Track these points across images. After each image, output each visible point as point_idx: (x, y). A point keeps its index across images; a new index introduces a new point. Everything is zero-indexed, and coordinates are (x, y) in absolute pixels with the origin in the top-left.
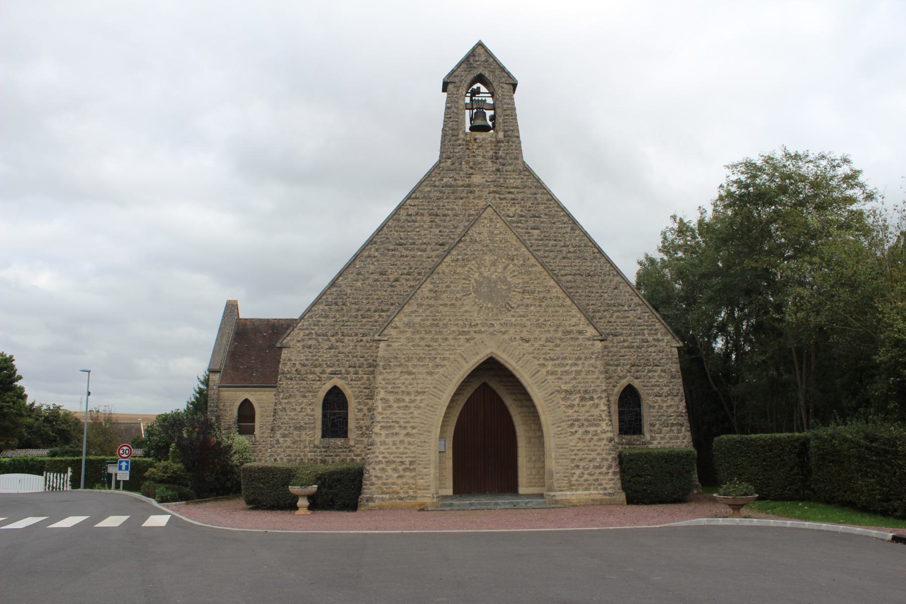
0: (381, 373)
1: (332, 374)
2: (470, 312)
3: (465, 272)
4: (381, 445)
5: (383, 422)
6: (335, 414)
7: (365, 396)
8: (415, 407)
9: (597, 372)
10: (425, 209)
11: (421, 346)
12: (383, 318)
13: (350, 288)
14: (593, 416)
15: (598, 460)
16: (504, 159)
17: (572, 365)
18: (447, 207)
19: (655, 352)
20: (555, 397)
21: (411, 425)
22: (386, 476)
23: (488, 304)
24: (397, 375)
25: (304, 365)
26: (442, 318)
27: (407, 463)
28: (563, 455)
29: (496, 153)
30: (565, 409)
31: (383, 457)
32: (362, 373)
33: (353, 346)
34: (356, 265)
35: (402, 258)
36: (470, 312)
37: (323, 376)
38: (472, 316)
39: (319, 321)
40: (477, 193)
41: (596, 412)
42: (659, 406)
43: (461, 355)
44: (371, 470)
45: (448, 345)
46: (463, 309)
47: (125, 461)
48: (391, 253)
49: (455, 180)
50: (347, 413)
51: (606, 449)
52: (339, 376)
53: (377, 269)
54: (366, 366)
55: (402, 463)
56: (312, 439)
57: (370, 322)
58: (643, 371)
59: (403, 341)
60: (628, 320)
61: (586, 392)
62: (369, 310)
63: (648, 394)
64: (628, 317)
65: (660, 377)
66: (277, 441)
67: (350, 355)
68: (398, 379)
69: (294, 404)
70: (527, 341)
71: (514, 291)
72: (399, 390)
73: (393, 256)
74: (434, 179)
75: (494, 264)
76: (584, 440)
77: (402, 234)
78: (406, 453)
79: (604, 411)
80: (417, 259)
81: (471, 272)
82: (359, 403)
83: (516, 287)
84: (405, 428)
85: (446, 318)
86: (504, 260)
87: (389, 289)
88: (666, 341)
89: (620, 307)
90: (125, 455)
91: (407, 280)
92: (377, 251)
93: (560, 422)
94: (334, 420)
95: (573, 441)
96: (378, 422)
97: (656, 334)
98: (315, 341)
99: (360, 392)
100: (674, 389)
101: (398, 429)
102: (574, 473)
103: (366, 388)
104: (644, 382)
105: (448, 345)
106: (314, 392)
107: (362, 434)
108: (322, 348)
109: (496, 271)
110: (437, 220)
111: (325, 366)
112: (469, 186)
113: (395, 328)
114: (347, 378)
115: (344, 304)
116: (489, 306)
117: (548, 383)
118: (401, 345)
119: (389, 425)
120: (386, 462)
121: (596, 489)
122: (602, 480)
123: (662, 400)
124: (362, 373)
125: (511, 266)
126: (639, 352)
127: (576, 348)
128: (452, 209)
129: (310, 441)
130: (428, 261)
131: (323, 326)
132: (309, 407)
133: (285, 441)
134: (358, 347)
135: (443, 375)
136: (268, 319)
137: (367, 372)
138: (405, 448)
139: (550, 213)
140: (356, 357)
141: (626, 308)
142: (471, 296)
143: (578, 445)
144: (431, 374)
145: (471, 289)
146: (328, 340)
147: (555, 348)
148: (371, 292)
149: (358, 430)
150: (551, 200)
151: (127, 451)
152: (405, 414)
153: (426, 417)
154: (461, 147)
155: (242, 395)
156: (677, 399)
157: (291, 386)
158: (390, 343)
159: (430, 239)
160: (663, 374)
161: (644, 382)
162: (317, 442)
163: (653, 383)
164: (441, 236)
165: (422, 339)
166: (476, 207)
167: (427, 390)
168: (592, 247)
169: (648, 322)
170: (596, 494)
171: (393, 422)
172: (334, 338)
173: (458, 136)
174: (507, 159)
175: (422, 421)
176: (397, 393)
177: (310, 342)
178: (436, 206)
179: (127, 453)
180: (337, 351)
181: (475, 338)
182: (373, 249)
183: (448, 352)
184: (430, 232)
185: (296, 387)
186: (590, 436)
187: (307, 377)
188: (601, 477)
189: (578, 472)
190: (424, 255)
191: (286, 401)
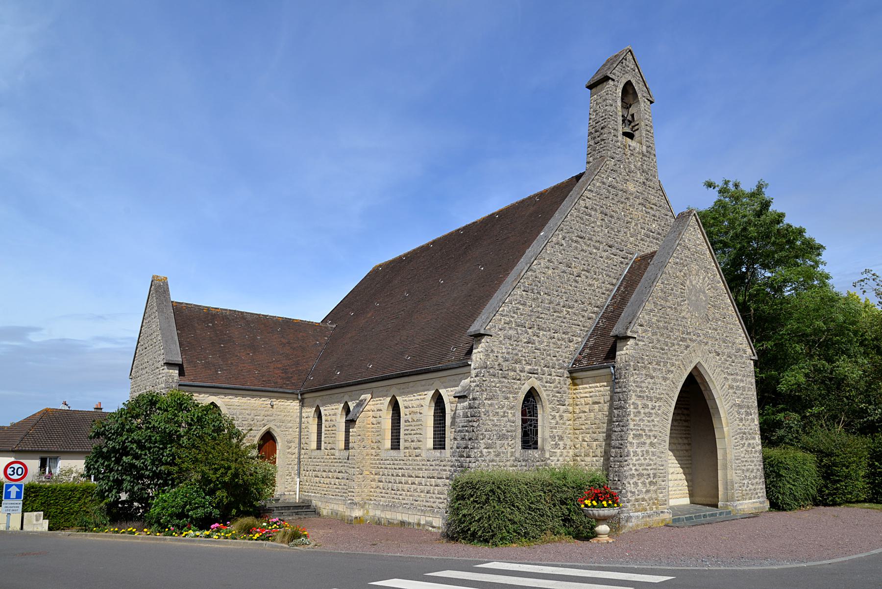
0: (632, 375)
1: (531, 373)
7: (558, 401)
27: (652, 475)
32: (555, 374)
37: (522, 374)
39: (518, 309)
47: (16, 485)
49: (617, 183)
52: (536, 376)
54: (557, 367)
56: (514, 450)
66: (481, 452)
69: (497, 407)
73: (576, 248)
87: (573, 284)
90: (15, 477)
92: (564, 239)
94: (525, 428)
96: (631, 429)
106: (515, 394)
107: (556, 444)
110: (606, 219)
111: (524, 362)
120: (638, 475)
124: (555, 374)
132: (510, 412)
140: (550, 355)
142: (686, 302)
146: (527, 332)
151: (20, 471)
157: (493, 384)
162: (517, 455)
167: (662, 396)
179: (20, 472)
180: (534, 346)
182: (561, 236)
185: (498, 385)
187: (508, 374)
190: (598, 254)
191: (489, 402)
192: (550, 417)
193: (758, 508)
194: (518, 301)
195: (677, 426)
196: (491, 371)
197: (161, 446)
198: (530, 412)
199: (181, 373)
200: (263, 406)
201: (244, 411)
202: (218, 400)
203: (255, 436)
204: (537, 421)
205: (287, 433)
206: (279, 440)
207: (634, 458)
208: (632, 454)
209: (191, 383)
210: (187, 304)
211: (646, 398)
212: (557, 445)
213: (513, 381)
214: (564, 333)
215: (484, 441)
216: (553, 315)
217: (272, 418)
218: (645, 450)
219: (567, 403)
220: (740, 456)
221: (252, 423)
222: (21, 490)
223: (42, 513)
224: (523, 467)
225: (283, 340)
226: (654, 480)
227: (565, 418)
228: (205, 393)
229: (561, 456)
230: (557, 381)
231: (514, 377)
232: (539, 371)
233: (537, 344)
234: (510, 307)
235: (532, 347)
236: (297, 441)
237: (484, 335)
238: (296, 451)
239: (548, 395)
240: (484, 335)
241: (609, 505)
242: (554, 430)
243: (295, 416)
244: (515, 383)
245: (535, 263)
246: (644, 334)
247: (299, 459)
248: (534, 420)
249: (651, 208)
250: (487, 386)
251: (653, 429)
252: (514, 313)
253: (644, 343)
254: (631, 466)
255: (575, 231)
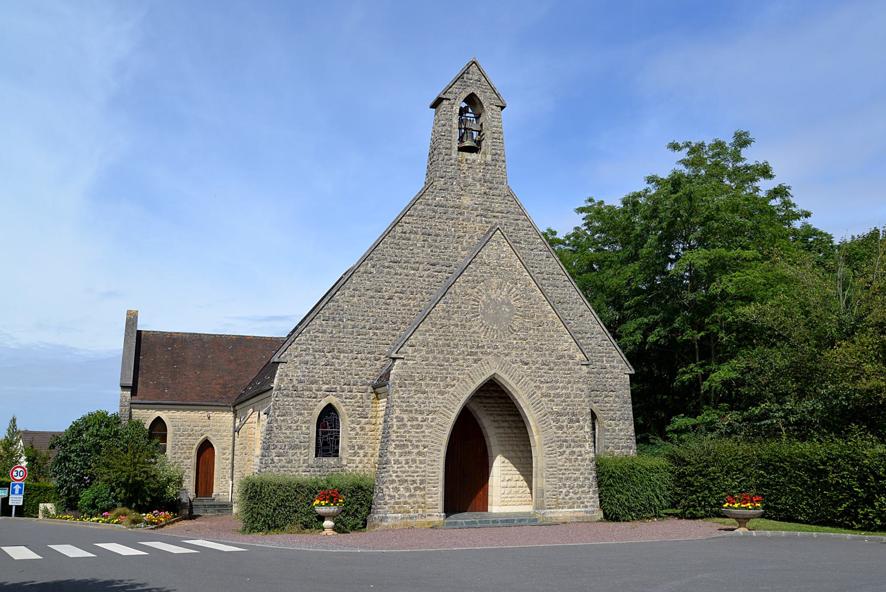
0: (397, 392)
2: (477, 333)
3: (475, 294)
4: (394, 464)
5: (397, 440)
6: (326, 433)
7: (359, 414)
8: (426, 426)
9: (583, 396)
10: (419, 228)
11: (434, 365)
12: (377, 335)
13: (347, 303)
14: (578, 437)
15: (581, 479)
16: (491, 183)
17: (564, 388)
18: (439, 227)
19: (611, 378)
20: (548, 418)
21: (423, 443)
22: (399, 495)
23: (493, 326)
24: (412, 393)
25: (300, 382)
26: (453, 338)
27: (418, 482)
28: (553, 474)
29: (484, 175)
30: (555, 430)
31: (396, 476)
32: (356, 391)
33: (348, 363)
34: (352, 280)
35: (396, 276)
36: (477, 333)
37: (318, 393)
38: (479, 337)
40: (466, 214)
41: (580, 433)
42: (613, 429)
43: (469, 375)
44: (384, 489)
45: (458, 365)
46: (472, 330)
48: (386, 270)
50: (166, 434)
51: (588, 469)
52: (334, 393)
53: (373, 285)
54: (360, 384)
55: (414, 482)
56: (307, 458)
57: (365, 339)
58: (601, 396)
59: (418, 360)
60: (590, 346)
61: (574, 414)
62: (364, 327)
63: (604, 417)
64: (590, 344)
65: (615, 402)
66: (272, 460)
67: (345, 372)
68: (412, 397)
69: (290, 422)
70: (526, 364)
71: (516, 315)
72: (413, 409)
73: (389, 273)
74: (427, 197)
75: (500, 287)
76: (570, 460)
77: (397, 251)
78: (417, 472)
79: (588, 432)
80: (410, 278)
81: (480, 294)
82: (353, 422)
83: (518, 311)
84: (417, 447)
85: (456, 338)
86: (508, 283)
88: (620, 368)
89: (584, 334)
90: (18, 478)
91: (401, 298)
92: (373, 267)
93: (552, 443)
94: (326, 438)
95: (561, 461)
97: (613, 361)
98: (312, 357)
99: (353, 411)
100: (625, 414)
101: (410, 447)
102: (562, 492)
103: (359, 407)
104: (601, 406)
105: (458, 365)
107: (355, 453)
108: (319, 364)
109: (501, 294)
110: (429, 240)
112: (459, 207)
113: (411, 346)
114: (342, 395)
115: (341, 320)
116: (494, 328)
117: (542, 405)
118: (416, 364)
119: (402, 443)
120: (399, 480)
121: (579, 507)
122: (584, 498)
123: (615, 424)
124: (356, 391)
125: (514, 289)
126: (599, 378)
127: (566, 372)
128: (443, 230)
129: (305, 460)
130: (420, 280)
131: (320, 341)
132: (304, 425)
133: (279, 460)
134: (353, 365)
135: (452, 394)
136: (200, 335)
137: (361, 391)
138: (417, 467)
139: (529, 240)
140: (351, 374)
141: (589, 335)
142: (479, 317)
143: (566, 464)
144: (441, 393)
145: (479, 310)
147: (549, 371)
148: (366, 309)
149: (350, 449)
150: (530, 227)
151: (21, 473)
152: (417, 433)
153: (437, 436)
154: (453, 167)
155: (153, 414)
156: (627, 422)
157: (287, 403)
158: (406, 362)
159: (423, 258)
160: (617, 399)
161: (601, 406)
162: (311, 462)
163: (608, 408)
164: (432, 255)
165: (435, 358)
166: (465, 229)
167: (438, 409)
168: (563, 275)
169: (606, 349)
170: (578, 512)
171: (406, 440)
172: (330, 354)
173: (450, 155)
174: (493, 183)
175: (433, 440)
176: (411, 411)
177: (307, 358)
178: (428, 225)
179: (21, 474)
180: (333, 367)
181: (481, 359)
182: (370, 265)
183: (458, 372)
184: (423, 251)
185: (292, 403)
186: (575, 456)
188: (583, 496)
189: (564, 491)
190: (417, 274)
191: (282, 418)
192: (349, 429)
193: (583, 517)
194: (316, 330)
195: (518, 433)
196: (285, 393)
197: (89, 454)
198: (330, 425)
199: (134, 394)
200: (201, 418)
201: (185, 423)
202: (164, 415)
203: (194, 444)
204: (339, 432)
205: (222, 441)
206: (215, 448)
207: (396, 466)
208: (393, 462)
209: (140, 401)
210: (154, 332)
211: (414, 412)
212: (355, 454)
213: (308, 399)
214: (369, 353)
215: (275, 450)
216: (357, 338)
217: (209, 428)
218: (410, 459)
219: (369, 416)
220: (556, 464)
221: (191, 433)
222: (22, 487)
223: (21, 504)
224: (316, 473)
225: (231, 357)
226: (422, 486)
227: (367, 429)
228: (152, 409)
229: (360, 463)
230: (359, 396)
231: (309, 396)
232: (338, 389)
233: (336, 365)
234: (308, 336)
235: (331, 369)
236: (231, 448)
237: (278, 363)
238: (230, 457)
239: (347, 410)
240: (278, 363)
241: (326, 505)
242: (353, 440)
243: (229, 426)
244: (309, 401)
245: (337, 294)
246: (415, 354)
247: (233, 464)
248: (335, 431)
249: (494, 216)
250: (280, 405)
251: (423, 439)
252: (312, 341)
253: (415, 362)
254: (391, 473)
255: (389, 257)
